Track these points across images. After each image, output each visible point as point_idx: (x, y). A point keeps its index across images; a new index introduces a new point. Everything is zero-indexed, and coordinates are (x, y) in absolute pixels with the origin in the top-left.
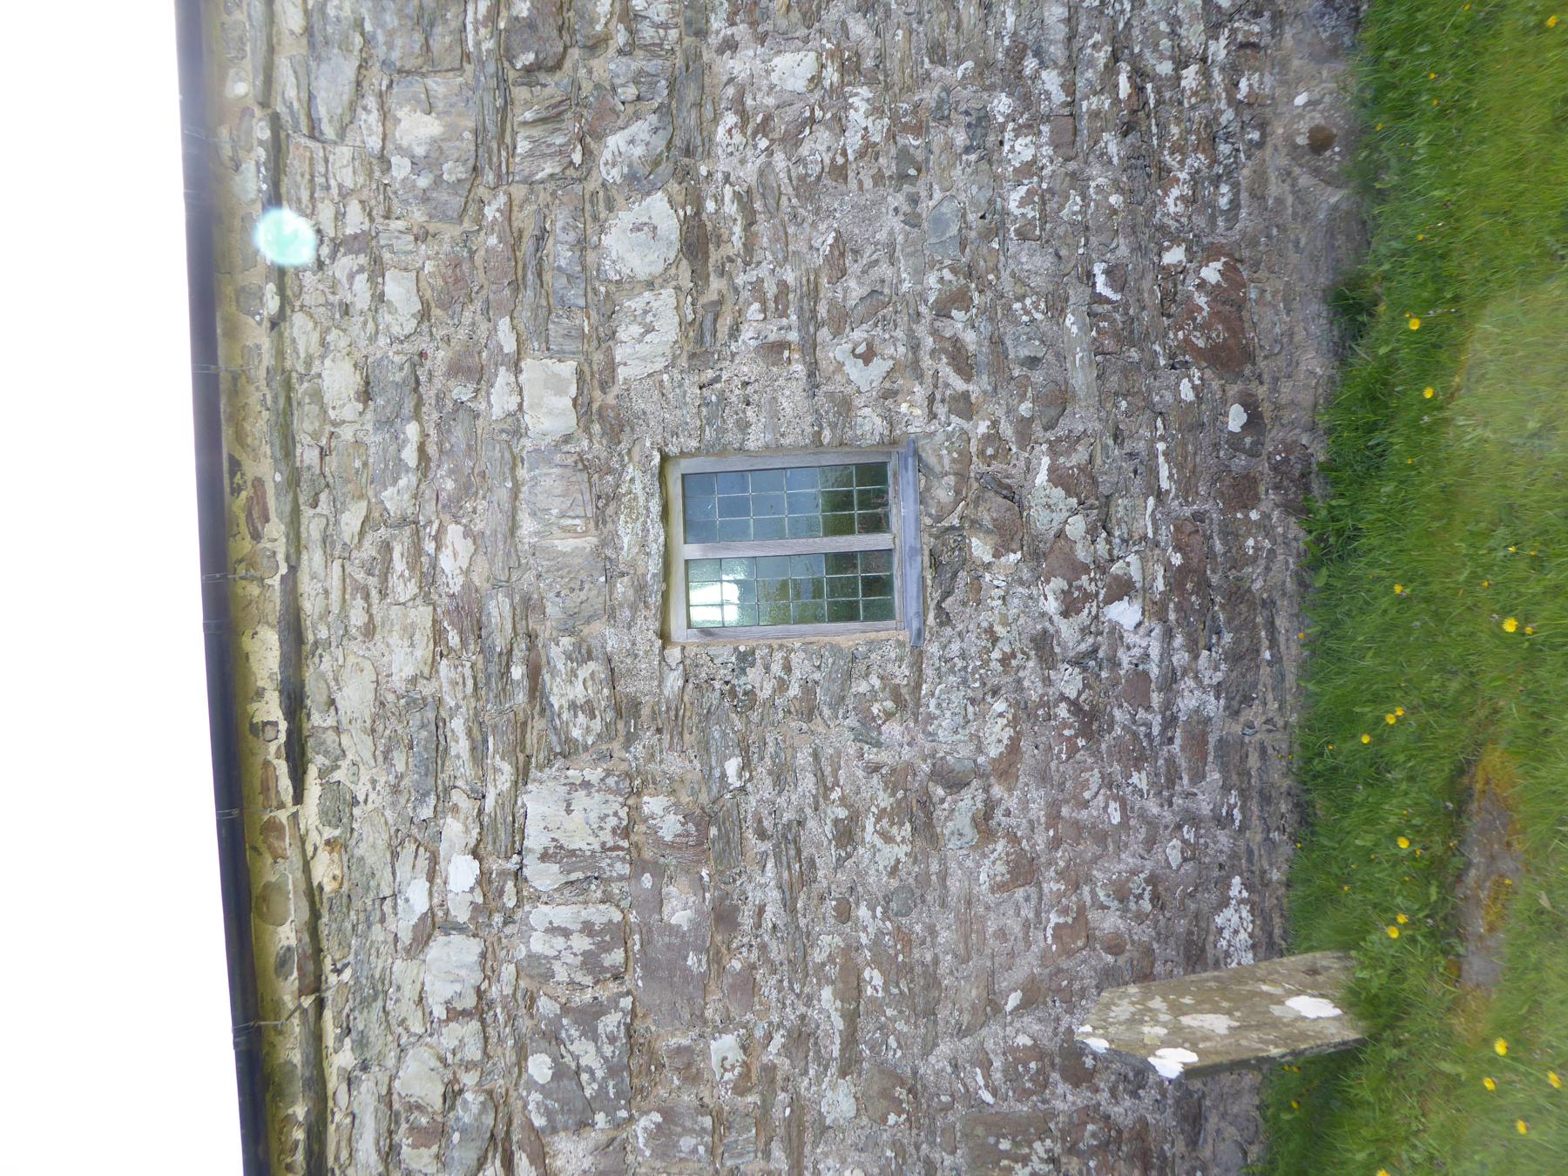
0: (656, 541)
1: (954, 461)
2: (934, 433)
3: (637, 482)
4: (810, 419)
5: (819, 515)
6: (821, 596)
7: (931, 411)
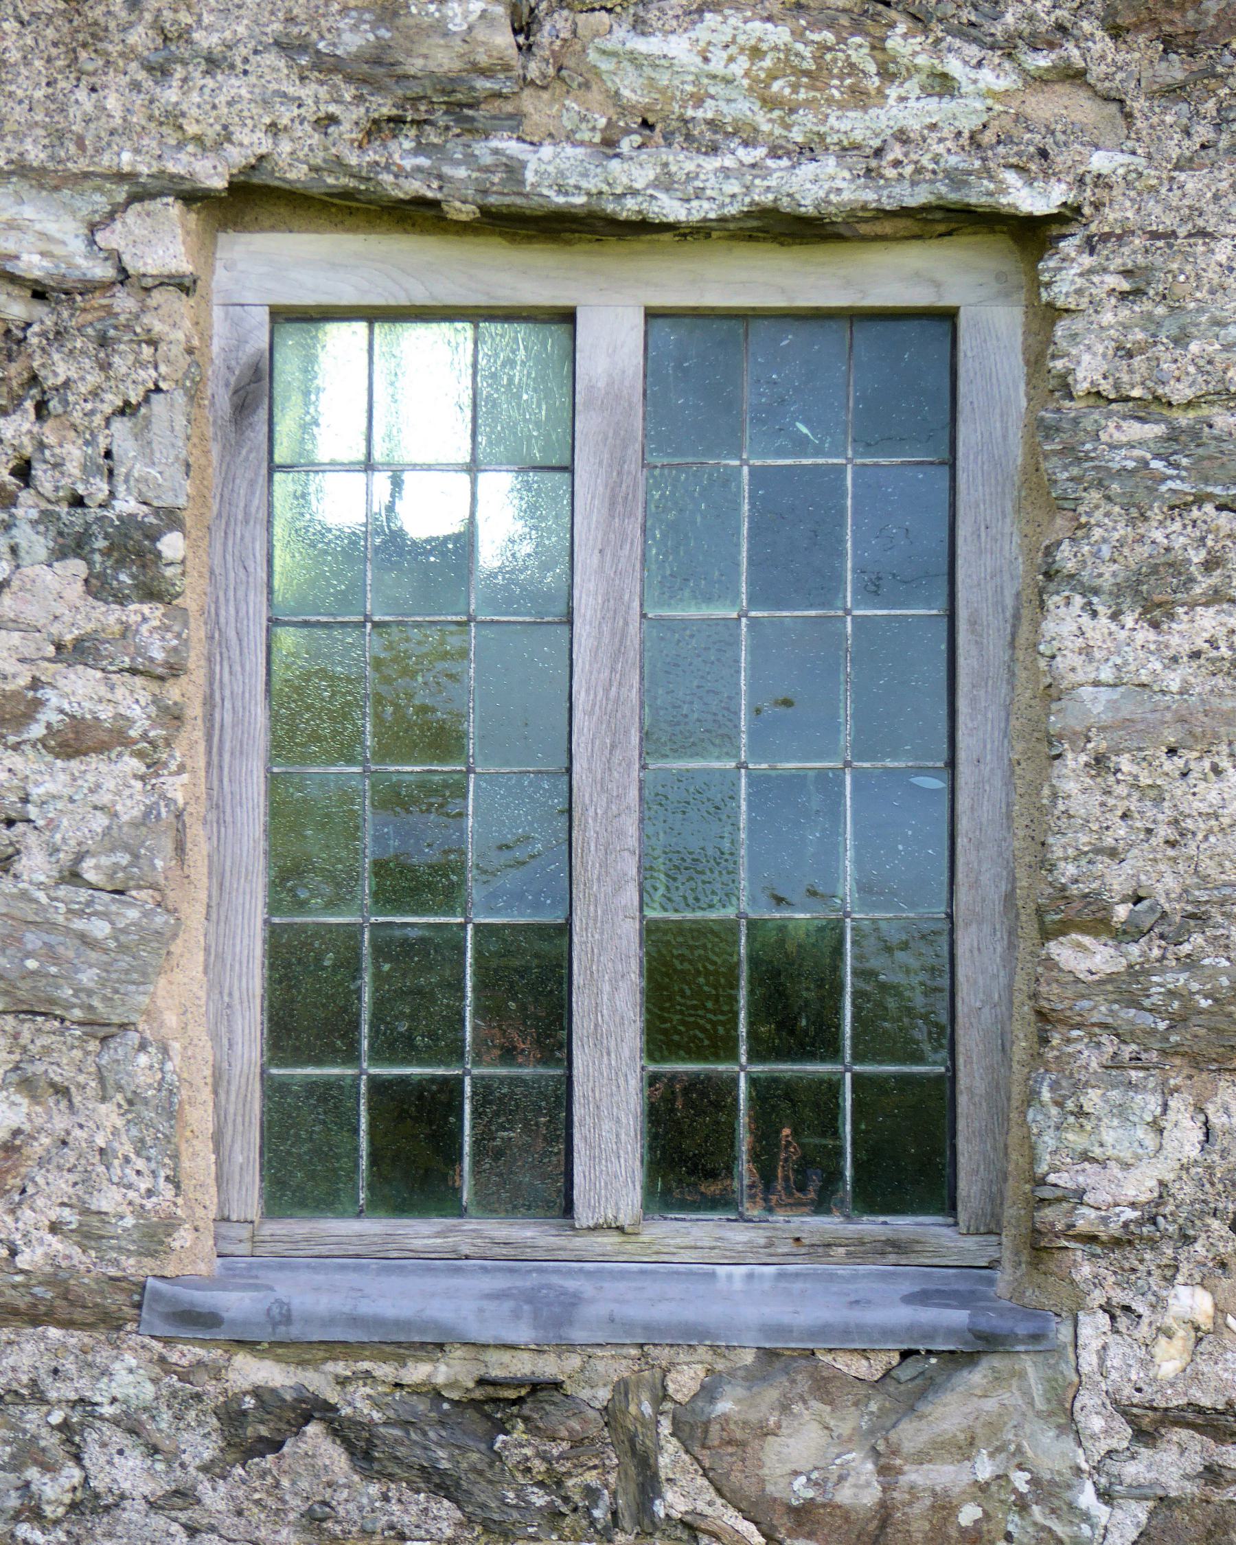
0: (666, 182)
1: (944, 1507)
2: (1067, 1420)
3: (936, 109)
4: (1166, 885)
5: (741, 904)
6: (386, 898)
7: (1171, 1418)
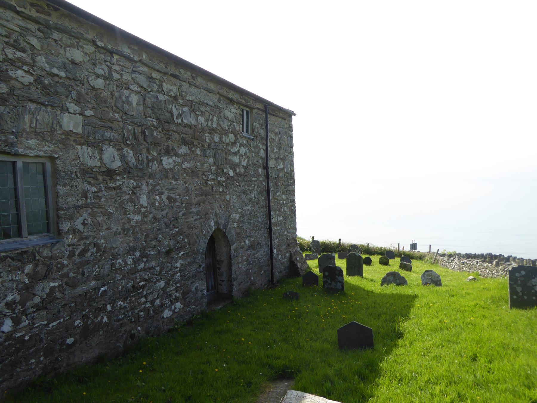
0: (30, 153)
1: (56, 254)
